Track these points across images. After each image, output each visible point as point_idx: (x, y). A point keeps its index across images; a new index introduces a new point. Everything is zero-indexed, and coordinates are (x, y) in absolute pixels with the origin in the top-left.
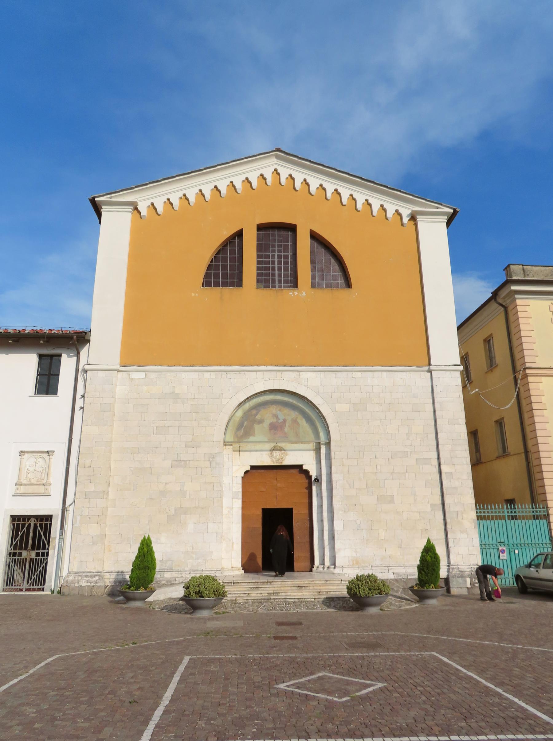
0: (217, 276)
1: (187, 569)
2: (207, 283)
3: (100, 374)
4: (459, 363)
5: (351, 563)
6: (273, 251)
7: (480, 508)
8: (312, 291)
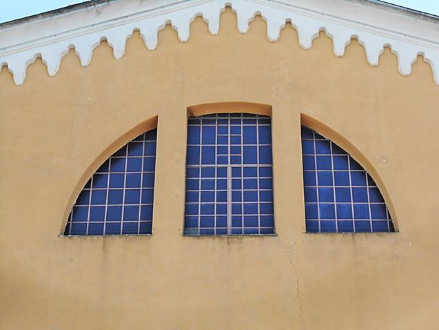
6: (223, 160)
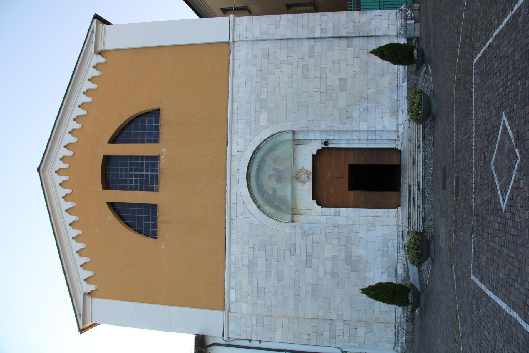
0: (147, 226)
1: (396, 255)
2: (154, 235)
3: (231, 327)
4: (228, 18)
5: (395, 117)
6: (126, 176)
7: (351, 7)
8: (161, 142)
